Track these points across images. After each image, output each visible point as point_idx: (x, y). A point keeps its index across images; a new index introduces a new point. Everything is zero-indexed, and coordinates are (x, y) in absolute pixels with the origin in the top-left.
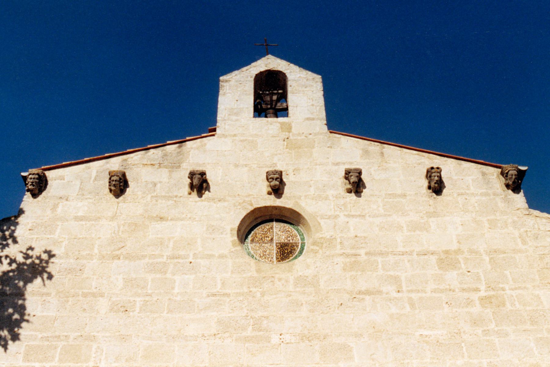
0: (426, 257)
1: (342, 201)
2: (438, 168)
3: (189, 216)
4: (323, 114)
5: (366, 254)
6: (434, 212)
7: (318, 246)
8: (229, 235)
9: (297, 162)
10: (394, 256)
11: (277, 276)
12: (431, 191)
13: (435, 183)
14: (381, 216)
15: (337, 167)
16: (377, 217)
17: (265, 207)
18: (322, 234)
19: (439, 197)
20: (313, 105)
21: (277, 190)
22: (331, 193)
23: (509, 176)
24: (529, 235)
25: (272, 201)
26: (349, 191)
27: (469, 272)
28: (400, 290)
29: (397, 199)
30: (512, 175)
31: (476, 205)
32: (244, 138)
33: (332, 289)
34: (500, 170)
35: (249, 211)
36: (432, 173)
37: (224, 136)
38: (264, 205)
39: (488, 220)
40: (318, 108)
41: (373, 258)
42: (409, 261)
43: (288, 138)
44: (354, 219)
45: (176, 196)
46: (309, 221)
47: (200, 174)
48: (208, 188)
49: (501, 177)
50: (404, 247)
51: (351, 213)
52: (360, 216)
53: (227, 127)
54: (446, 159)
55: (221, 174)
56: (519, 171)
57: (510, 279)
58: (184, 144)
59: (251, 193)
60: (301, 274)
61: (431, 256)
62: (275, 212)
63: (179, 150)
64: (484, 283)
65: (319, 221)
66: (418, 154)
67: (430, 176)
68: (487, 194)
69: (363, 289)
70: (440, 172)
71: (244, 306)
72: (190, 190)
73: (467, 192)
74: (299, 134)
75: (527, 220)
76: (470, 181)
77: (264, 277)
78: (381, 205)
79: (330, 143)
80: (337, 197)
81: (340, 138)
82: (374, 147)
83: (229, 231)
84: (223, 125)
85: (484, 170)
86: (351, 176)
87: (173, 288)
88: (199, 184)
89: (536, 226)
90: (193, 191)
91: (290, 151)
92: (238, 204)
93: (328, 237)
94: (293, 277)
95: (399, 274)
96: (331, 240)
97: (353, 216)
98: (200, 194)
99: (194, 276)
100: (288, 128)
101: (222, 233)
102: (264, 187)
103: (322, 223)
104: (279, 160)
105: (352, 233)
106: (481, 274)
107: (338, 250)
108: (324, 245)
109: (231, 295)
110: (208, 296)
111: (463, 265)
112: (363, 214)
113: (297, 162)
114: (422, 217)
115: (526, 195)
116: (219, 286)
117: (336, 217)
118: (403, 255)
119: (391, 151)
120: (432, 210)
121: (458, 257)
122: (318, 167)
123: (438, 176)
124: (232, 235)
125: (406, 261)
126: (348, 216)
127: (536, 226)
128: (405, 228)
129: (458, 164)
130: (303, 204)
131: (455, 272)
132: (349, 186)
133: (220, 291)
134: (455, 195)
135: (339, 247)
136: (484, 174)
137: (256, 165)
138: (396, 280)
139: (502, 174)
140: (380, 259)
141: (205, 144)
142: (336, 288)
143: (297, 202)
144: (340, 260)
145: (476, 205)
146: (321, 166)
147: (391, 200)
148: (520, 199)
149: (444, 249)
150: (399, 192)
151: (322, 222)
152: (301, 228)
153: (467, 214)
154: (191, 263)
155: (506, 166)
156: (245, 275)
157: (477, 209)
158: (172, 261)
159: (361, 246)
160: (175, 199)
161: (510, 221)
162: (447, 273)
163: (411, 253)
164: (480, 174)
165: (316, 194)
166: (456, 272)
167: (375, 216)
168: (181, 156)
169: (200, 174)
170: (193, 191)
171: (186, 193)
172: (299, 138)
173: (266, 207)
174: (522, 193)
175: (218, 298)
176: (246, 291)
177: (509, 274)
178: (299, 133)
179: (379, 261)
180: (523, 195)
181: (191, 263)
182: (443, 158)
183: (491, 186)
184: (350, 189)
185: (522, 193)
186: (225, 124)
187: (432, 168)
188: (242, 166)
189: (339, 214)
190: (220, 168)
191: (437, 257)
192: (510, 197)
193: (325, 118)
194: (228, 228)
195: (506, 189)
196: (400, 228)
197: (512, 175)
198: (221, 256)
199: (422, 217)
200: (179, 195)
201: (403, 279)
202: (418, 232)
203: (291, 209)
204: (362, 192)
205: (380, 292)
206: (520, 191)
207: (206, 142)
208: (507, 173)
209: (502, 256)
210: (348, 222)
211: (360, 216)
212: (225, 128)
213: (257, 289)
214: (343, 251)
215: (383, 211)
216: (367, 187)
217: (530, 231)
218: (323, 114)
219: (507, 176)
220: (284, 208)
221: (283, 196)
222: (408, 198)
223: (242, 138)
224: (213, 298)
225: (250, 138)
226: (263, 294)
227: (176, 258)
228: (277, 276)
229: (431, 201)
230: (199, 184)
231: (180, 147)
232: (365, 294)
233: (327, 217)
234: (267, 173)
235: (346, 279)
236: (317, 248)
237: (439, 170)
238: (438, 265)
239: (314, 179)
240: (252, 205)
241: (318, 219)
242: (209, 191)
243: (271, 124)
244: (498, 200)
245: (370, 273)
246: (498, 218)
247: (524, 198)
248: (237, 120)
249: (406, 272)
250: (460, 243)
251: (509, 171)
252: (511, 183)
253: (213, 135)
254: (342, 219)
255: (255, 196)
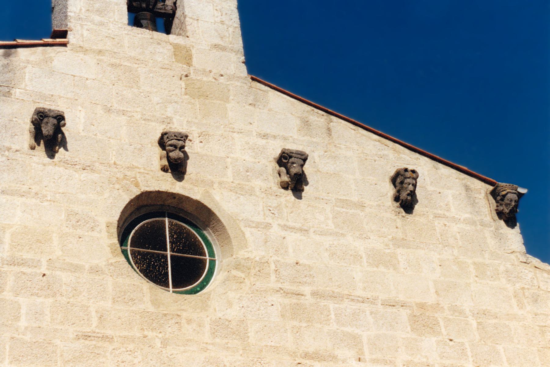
0: (394, 310)
1: (274, 202)
2: (413, 171)
3: (35, 189)
4: (239, 44)
5: (314, 294)
6: (403, 239)
7: (243, 272)
8: (104, 234)
9: (204, 122)
10: (351, 303)
11: (184, 314)
12: (398, 204)
13: (408, 195)
14: (331, 234)
15: (264, 141)
16: (326, 235)
17: (159, 192)
18: (248, 252)
19: (408, 216)
20: (222, 22)
21: (177, 168)
22: (258, 183)
23: (506, 201)
24: (526, 294)
25: (167, 184)
26: (285, 186)
27: (451, 340)
28: (361, 357)
29: (353, 211)
30: (511, 201)
31: (458, 236)
32: (118, 61)
33: (267, 346)
34: (491, 188)
35: (133, 197)
36: (406, 178)
37: (82, 49)
38: (157, 189)
39: (475, 263)
40: (231, 30)
41: (323, 303)
42: (371, 313)
43: (187, 76)
44: (293, 234)
45: (9, 149)
46: (227, 227)
47: (55, 118)
48: (63, 144)
49: (491, 198)
50: (364, 289)
51: (288, 224)
52: (301, 230)
53: (85, 33)
54: (417, 155)
55: (83, 121)
56: (520, 195)
57: (504, 359)
58: (13, 50)
59: (136, 164)
60: (220, 315)
61: (401, 309)
62: (169, 201)
63: (5, 61)
64: (471, 359)
65: (243, 229)
66: (379, 141)
67: (402, 183)
68: (473, 223)
69: (311, 350)
70: (415, 179)
71: (136, 361)
72: (33, 141)
73: (447, 214)
74: (205, 72)
75: (523, 270)
76: (450, 198)
77: (165, 315)
78: (331, 216)
79: (252, 98)
80: (267, 192)
81: (267, 92)
82: (318, 118)
83: (103, 227)
84: (79, 28)
85: (469, 183)
86: (293, 163)
87: (17, 318)
88: (49, 133)
89: (535, 282)
90: (39, 144)
91: (193, 101)
92: (114, 179)
93: (257, 259)
94: (208, 319)
95: (357, 331)
96: (264, 263)
97: (292, 229)
98: (51, 152)
99: (51, 300)
100: (184, 56)
101: (92, 229)
102: (155, 157)
103: (248, 235)
104: (176, 112)
105: (291, 260)
106: (467, 345)
107: (273, 283)
108: (253, 271)
109: (115, 339)
110: (78, 338)
111: (443, 330)
112: (306, 228)
113: (204, 122)
114: (387, 245)
115: (523, 233)
116: (95, 321)
117: (268, 226)
118: (363, 302)
119: (340, 126)
120: (400, 235)
121: (436, 315)
122: (235, 135)
123: (413, 185)
124: (110, 235)
125: (368, 313)
126: (285, 227)
127: (535, 282)
128: (364, 259)
129: (435, 167)
130: (217, 198)
131: (434, 339)
132: (286, 178)
133: (97, 331)
134: (431, 217)
135: (273, 277)
136: (467, 188)
137: (139, 116)
138: (354, 341)
139: (494, 194)
140: (332, 305)
141: (52, 60)
142: (273, 344)
143: (208, 192)
144: (276, 299)
145: (458, 236)
146: (241, 135)
147: (344, 210)
148: (514, 237)
149: (418, 300)
150: (355, 199)
151: (248, 232)
152: (210, 234)
153: (446, 248)
154: (44, 275)
155: (504, 184)
156: (134, 308)
157: (460, 243)
158: (12, 268)
159: (305, 280)
160: (7, 153)
161: (502, 268)
162: (424, 338)
163: (372, 301)
164: (463, 188)
165: (237, 182)
166: (435, 339)
167: (322, 233)
168: (10, 74)
169: (55, 118)
170: (39, 144)
171: (26, 146)
172: (205, 79)
173: (159, 193)
174: (517, 229)
175: (94, 343)
176: (138, 335)
177: (503, 350)
178: (204, 70)
179: (331, 309)
180: (519, 231)
181: (44, 275)
182: (413, 153)
183: (477, 209)
184: (287, 182)
185: (517, 229)
186: (82, 26)
187: (406, 170)
188: (117, 113)
189: (270, 221)
190: (80, 108)
191: (409, 312)
192: (501, 231)
193: (242, 50)
194: (103, 221)
195: (496, 217)
196: (357, 258)
197: (511, 201)
198: (95, 270)
199: (387, 245)
200: (14, 147)
201: (365, 340)
202: (382, 269)
203: (199, 202)
204: (303, 190)
205: (334, 358)
206: (516, 225)
207: (52, 55)
208: (504, 196)
209: (494, 321)
210: (284, 238)
211: (301, 230)
212: (82, 35)
213: (155, 334)
214: (280, 285)
215: (333, 227)
216: (310, 184)
217: (528, 289)
218: (238, 43)
219: (502, 200)
220: (188, 198)
221: (186, 177)
222: (367, 210)
223: (113, 61)
224: (87, 342)
225: (126, 64)
226: (165, 343)
227: (19, 264)
228: (184, 314)
229: (398, 220)
230: (49, 133)
231: (7, 55)
232: (313, 358)
233: (254, 225)
234: (163, 135)
235: (286, 331)
236: (243, 275)
237: (414, 175)
238: (410, 325)
239: (232, 155)
240: (137, 185)
241: (242, 225)
242: (66, 149)
243: (159, 44)
244: (487, 233)
245: (319, 326)
246: (487, 262)
247: (521, 236)
248: (102, 24)
249: (368, 330)
250: (438, 295)
251: (507, 194)
252: (507, 211)
253: (64, 45)
254: (275, 231)
255: (142, 171)
